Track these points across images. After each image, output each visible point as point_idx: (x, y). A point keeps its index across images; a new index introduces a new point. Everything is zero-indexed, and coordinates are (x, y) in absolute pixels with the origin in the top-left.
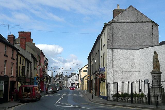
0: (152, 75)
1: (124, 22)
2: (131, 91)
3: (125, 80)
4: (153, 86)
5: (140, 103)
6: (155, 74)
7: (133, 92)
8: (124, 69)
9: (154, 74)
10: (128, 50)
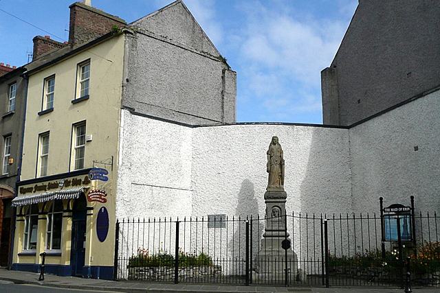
0: (266, 202)
1: (163, 40)
3: (157, 215)
5: (176, 281)
6: (278, 200)
7: (255, 250)
9: (274, 198)
10: (167, 123)
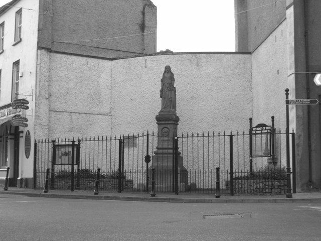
0: (158, 124)
2: (118, 164)
4: (161, 151)
6: (167, 122)
8: (76, 107)
9: (166, 120)
